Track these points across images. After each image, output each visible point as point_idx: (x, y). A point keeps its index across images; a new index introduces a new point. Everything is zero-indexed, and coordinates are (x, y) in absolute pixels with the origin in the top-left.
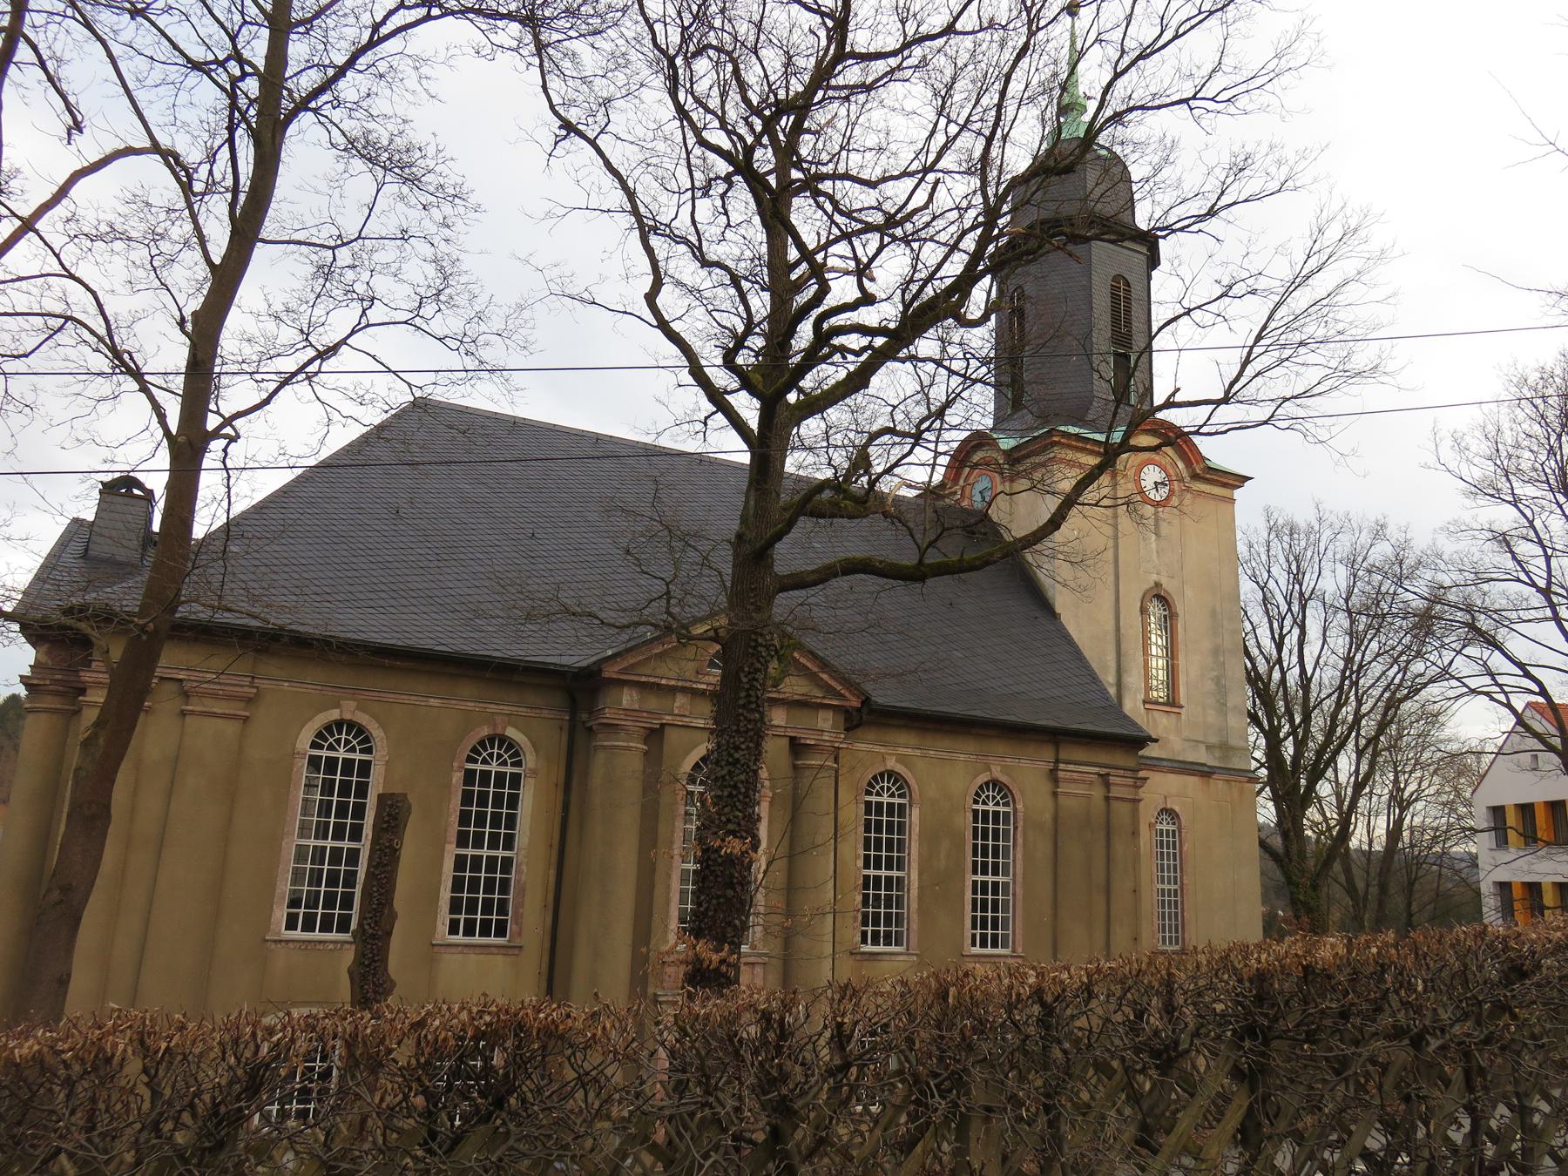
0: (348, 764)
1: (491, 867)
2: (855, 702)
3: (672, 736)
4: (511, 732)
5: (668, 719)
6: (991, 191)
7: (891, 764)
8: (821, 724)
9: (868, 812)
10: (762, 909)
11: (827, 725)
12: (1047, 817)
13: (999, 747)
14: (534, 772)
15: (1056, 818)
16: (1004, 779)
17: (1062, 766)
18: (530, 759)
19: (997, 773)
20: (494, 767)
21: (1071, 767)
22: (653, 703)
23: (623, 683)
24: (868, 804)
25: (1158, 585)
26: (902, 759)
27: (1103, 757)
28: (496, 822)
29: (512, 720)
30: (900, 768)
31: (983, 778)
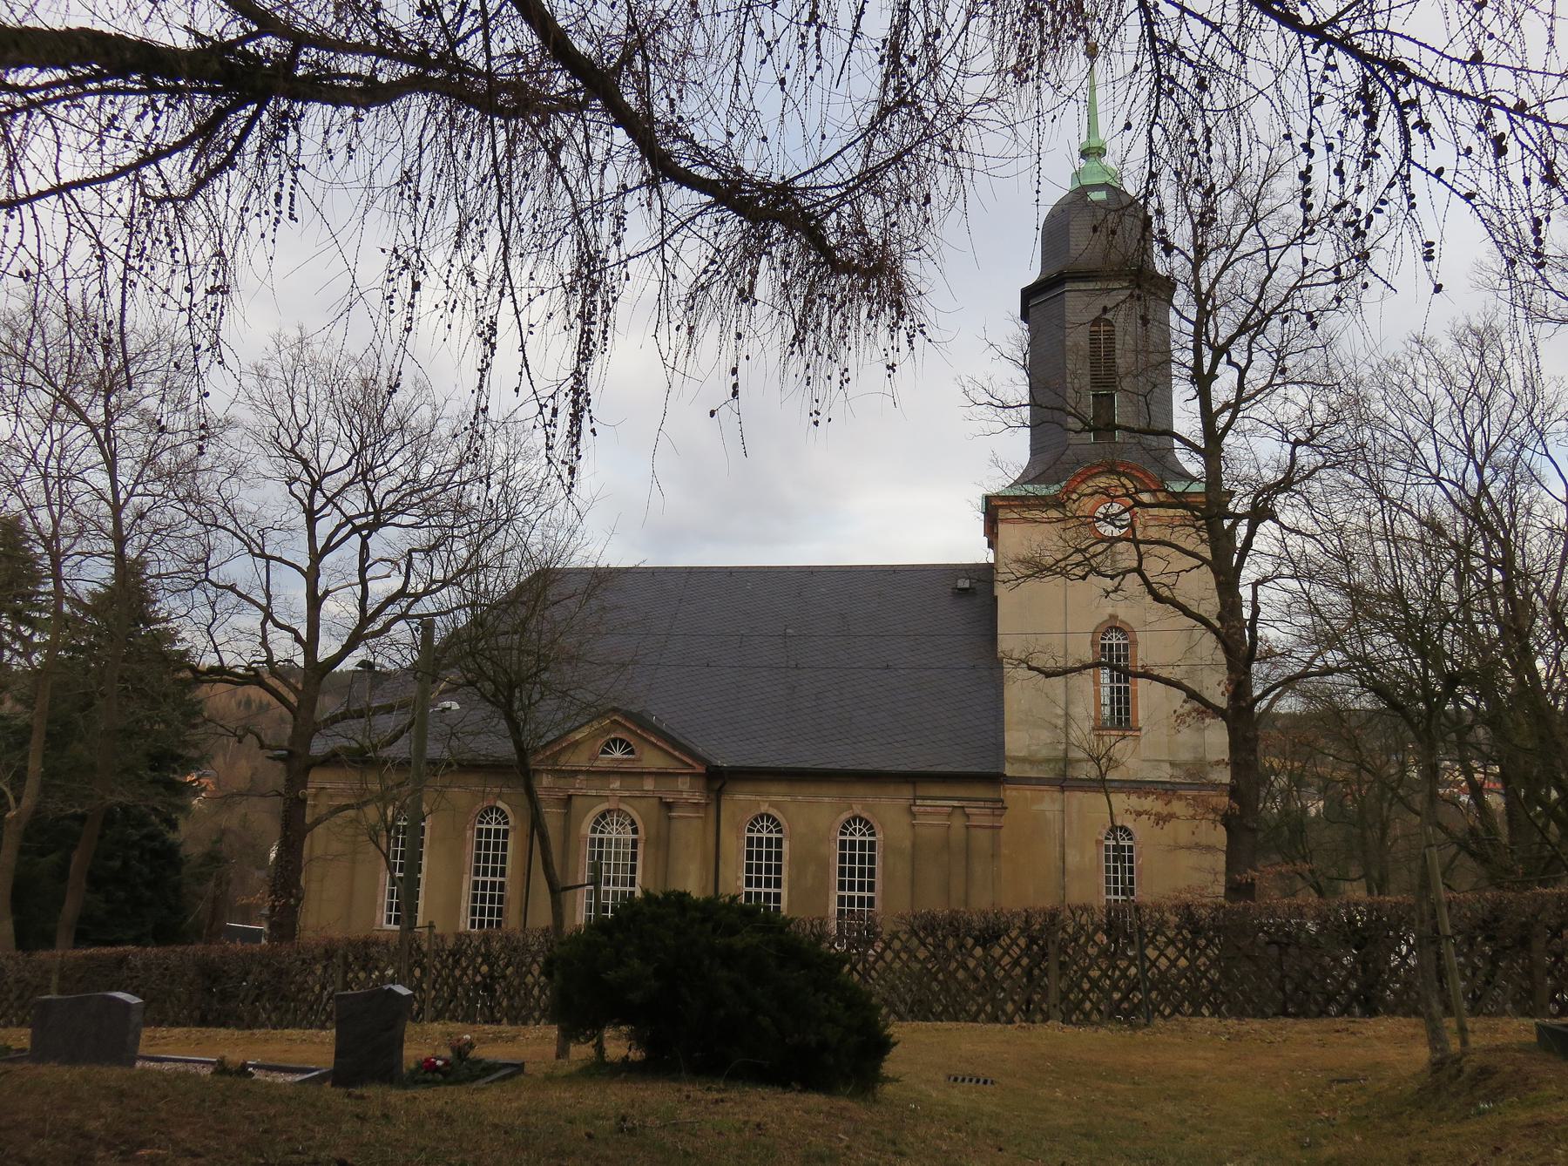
0: (769, 840)
1: (852, 884)
2: (700, 769)
3: (576, 802)
4: (500, 804)
5: (571, 791)
6: (1460, 445)
7: (764, 808)
8: (680, 787)
9: (480, 836)
10: (1449, 932)
11: (686, 787)
12: (907, 844)
13: (860, 790)
14: (514, 828)
15: (914, 845)
16: (864, 815)
17: (919, 802)
18: (511, 819)
19: (857, 809)
20: (857, 838)
21: (929, 802)
22: (561, 782)
23: (541, 772)
24: (480, 830)
25: (1113, 617)
26: (772, 804)
27: (961, 791)
28: (862, 860)
29: (499, 796)
30: (773, 812)
31: (846, 815)
